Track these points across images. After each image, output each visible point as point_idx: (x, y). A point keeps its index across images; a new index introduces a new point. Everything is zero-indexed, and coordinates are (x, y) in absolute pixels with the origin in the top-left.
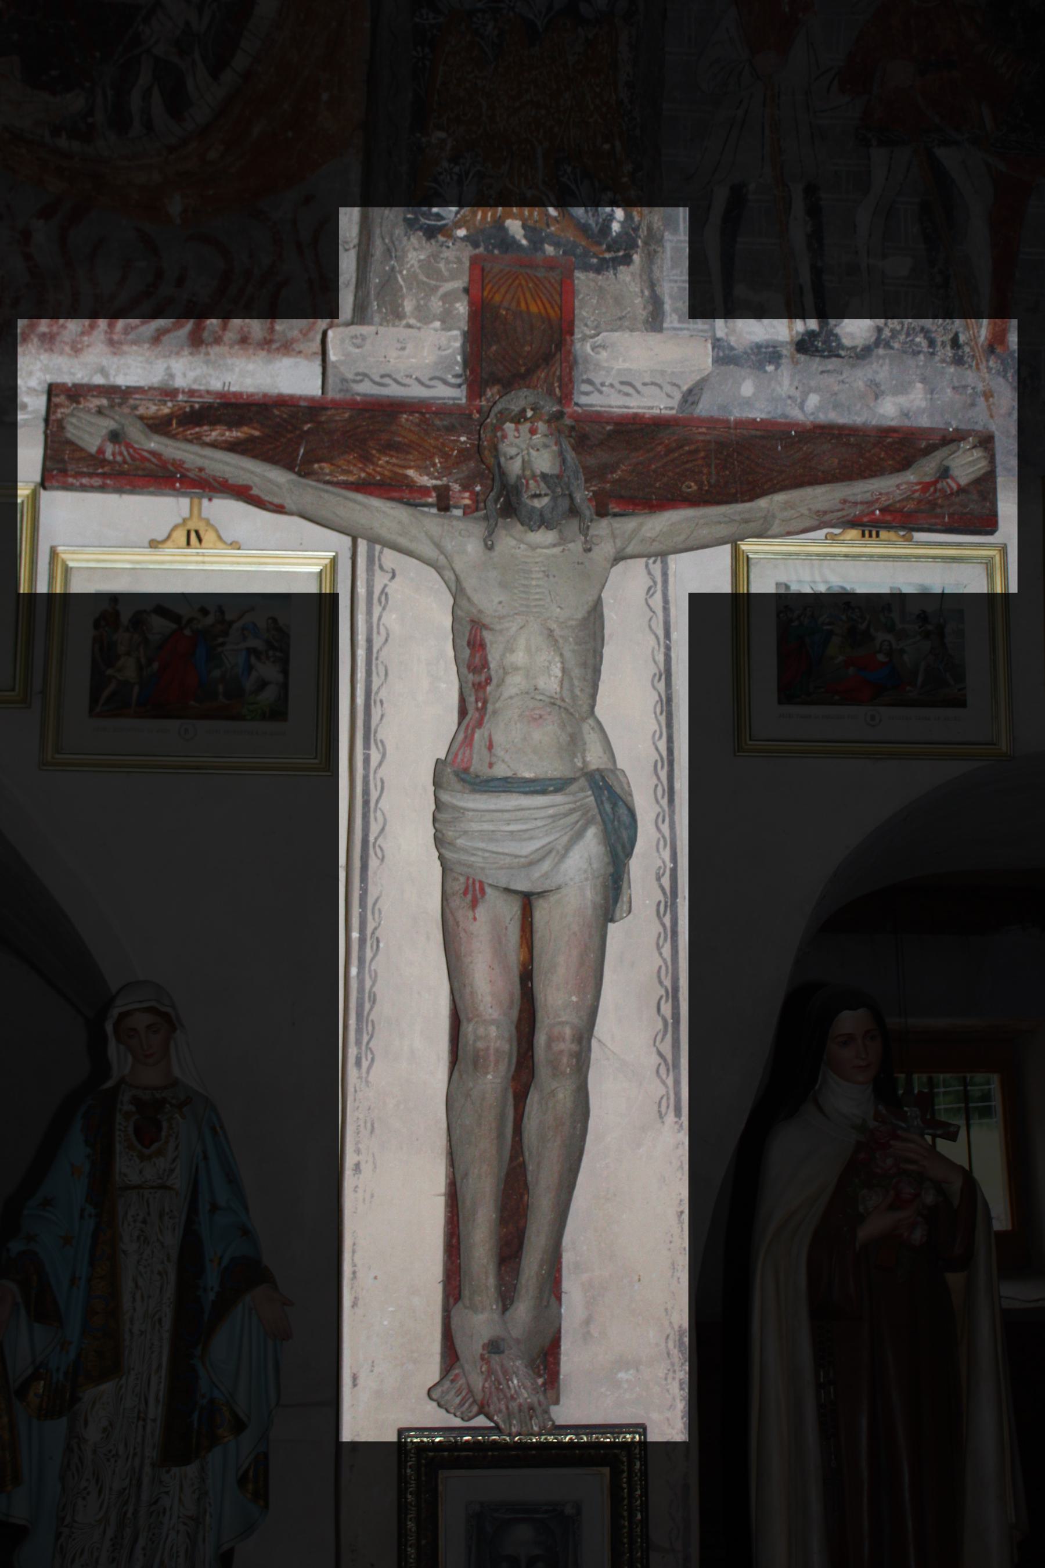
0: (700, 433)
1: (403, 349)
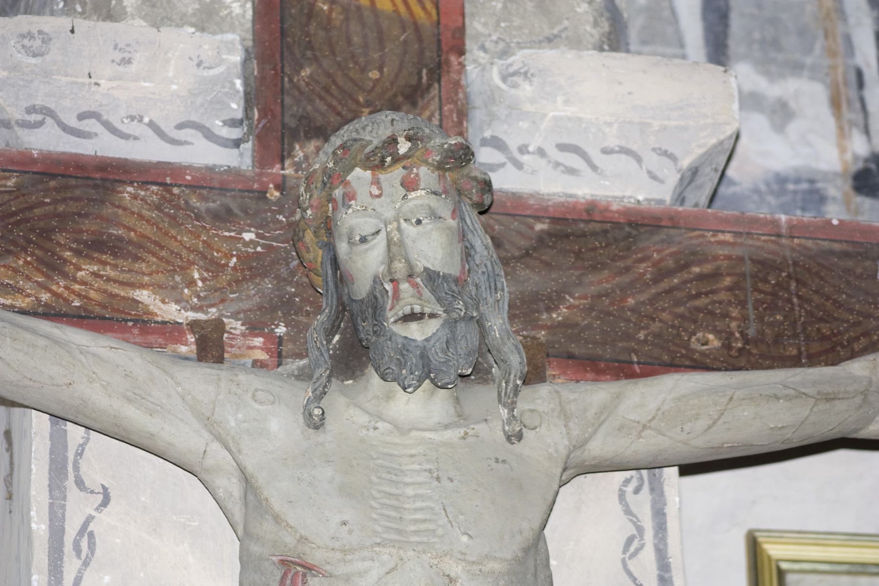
0: (720, 243)
1: (127, 62)
